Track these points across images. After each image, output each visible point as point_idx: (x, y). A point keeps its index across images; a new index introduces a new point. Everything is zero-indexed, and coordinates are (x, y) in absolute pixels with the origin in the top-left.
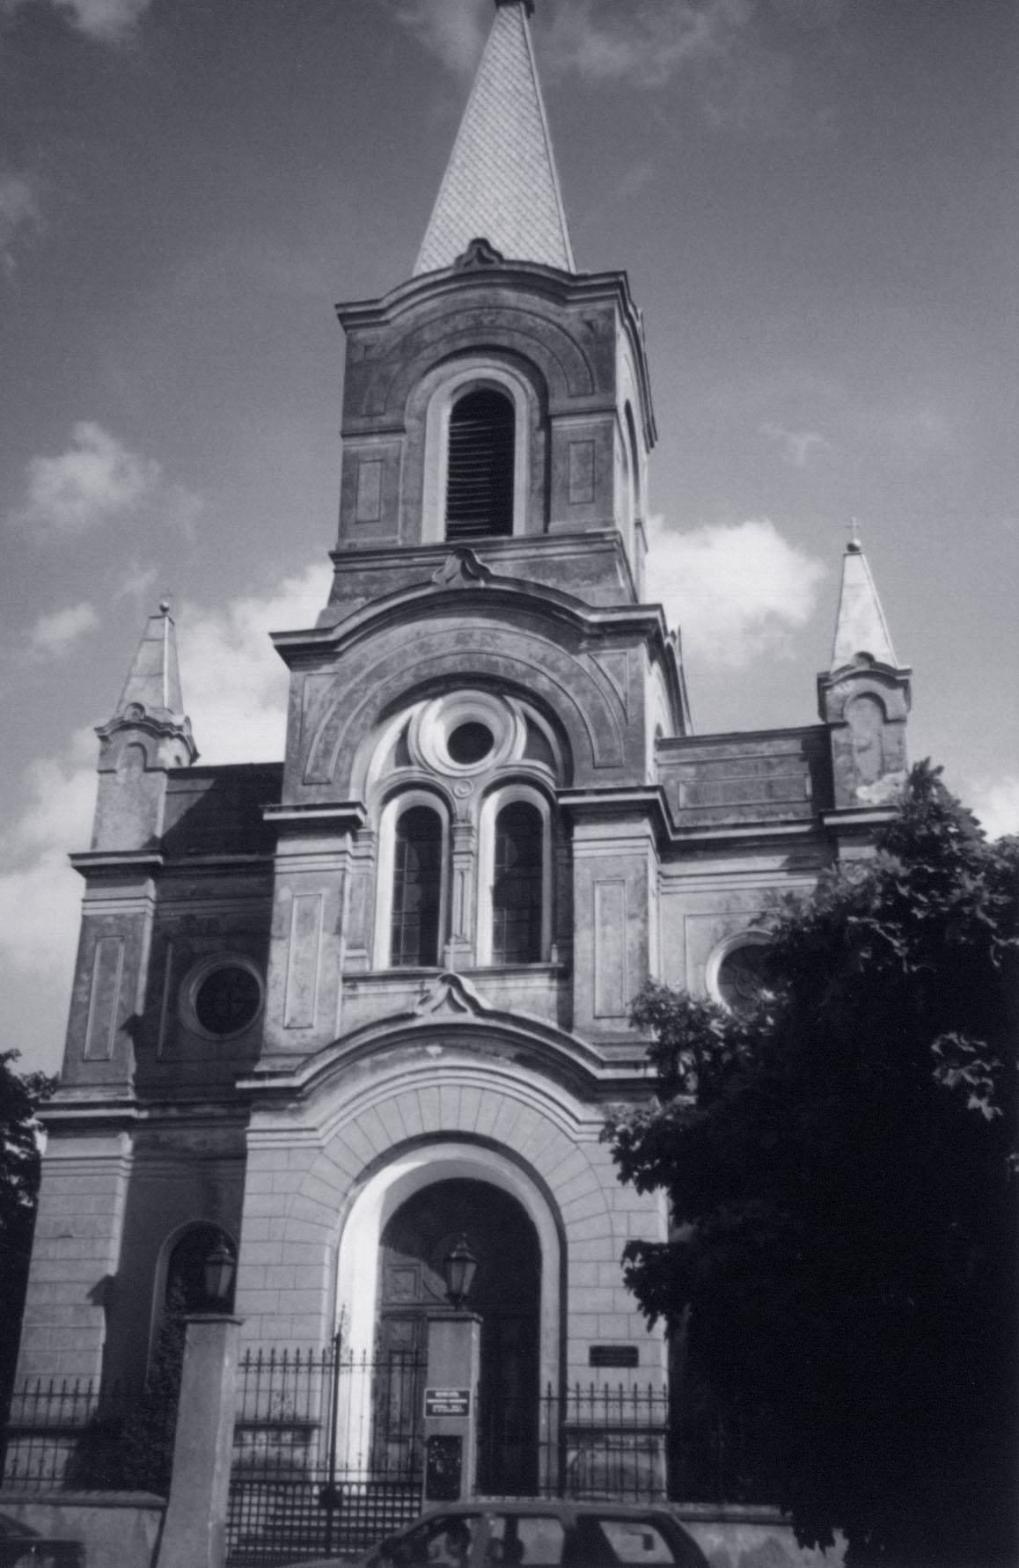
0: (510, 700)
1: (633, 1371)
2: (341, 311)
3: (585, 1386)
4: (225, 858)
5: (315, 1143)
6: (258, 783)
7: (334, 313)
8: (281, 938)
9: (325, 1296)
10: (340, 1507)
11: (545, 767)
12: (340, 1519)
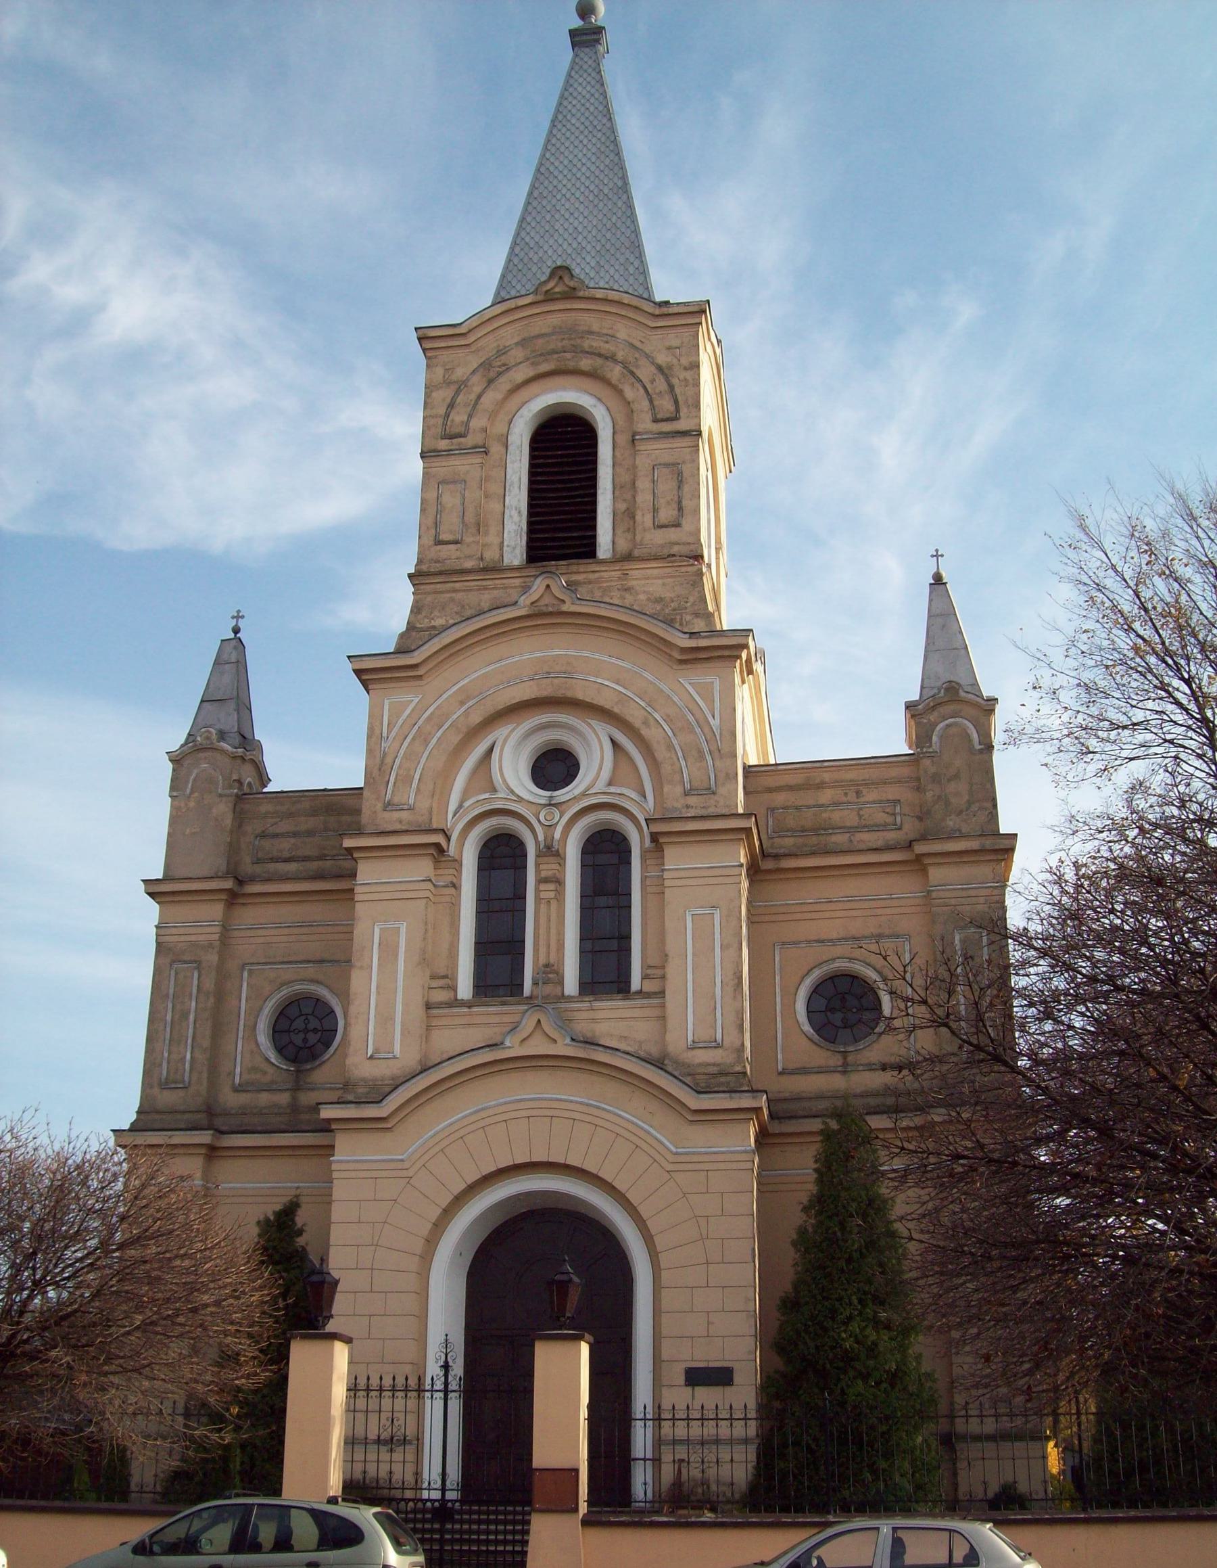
0: (593, 722)
1: (728, 1389)
2: (421, 332)
3: (681, 1406)
4: (747, 1025)
5: (405, 1173)
6: (334, 808)
7: (414, 336)
8: (361, 968)
9: (43, 1503)
10: (454, 1522)
11: (633, 795)
12: (453, 1531)
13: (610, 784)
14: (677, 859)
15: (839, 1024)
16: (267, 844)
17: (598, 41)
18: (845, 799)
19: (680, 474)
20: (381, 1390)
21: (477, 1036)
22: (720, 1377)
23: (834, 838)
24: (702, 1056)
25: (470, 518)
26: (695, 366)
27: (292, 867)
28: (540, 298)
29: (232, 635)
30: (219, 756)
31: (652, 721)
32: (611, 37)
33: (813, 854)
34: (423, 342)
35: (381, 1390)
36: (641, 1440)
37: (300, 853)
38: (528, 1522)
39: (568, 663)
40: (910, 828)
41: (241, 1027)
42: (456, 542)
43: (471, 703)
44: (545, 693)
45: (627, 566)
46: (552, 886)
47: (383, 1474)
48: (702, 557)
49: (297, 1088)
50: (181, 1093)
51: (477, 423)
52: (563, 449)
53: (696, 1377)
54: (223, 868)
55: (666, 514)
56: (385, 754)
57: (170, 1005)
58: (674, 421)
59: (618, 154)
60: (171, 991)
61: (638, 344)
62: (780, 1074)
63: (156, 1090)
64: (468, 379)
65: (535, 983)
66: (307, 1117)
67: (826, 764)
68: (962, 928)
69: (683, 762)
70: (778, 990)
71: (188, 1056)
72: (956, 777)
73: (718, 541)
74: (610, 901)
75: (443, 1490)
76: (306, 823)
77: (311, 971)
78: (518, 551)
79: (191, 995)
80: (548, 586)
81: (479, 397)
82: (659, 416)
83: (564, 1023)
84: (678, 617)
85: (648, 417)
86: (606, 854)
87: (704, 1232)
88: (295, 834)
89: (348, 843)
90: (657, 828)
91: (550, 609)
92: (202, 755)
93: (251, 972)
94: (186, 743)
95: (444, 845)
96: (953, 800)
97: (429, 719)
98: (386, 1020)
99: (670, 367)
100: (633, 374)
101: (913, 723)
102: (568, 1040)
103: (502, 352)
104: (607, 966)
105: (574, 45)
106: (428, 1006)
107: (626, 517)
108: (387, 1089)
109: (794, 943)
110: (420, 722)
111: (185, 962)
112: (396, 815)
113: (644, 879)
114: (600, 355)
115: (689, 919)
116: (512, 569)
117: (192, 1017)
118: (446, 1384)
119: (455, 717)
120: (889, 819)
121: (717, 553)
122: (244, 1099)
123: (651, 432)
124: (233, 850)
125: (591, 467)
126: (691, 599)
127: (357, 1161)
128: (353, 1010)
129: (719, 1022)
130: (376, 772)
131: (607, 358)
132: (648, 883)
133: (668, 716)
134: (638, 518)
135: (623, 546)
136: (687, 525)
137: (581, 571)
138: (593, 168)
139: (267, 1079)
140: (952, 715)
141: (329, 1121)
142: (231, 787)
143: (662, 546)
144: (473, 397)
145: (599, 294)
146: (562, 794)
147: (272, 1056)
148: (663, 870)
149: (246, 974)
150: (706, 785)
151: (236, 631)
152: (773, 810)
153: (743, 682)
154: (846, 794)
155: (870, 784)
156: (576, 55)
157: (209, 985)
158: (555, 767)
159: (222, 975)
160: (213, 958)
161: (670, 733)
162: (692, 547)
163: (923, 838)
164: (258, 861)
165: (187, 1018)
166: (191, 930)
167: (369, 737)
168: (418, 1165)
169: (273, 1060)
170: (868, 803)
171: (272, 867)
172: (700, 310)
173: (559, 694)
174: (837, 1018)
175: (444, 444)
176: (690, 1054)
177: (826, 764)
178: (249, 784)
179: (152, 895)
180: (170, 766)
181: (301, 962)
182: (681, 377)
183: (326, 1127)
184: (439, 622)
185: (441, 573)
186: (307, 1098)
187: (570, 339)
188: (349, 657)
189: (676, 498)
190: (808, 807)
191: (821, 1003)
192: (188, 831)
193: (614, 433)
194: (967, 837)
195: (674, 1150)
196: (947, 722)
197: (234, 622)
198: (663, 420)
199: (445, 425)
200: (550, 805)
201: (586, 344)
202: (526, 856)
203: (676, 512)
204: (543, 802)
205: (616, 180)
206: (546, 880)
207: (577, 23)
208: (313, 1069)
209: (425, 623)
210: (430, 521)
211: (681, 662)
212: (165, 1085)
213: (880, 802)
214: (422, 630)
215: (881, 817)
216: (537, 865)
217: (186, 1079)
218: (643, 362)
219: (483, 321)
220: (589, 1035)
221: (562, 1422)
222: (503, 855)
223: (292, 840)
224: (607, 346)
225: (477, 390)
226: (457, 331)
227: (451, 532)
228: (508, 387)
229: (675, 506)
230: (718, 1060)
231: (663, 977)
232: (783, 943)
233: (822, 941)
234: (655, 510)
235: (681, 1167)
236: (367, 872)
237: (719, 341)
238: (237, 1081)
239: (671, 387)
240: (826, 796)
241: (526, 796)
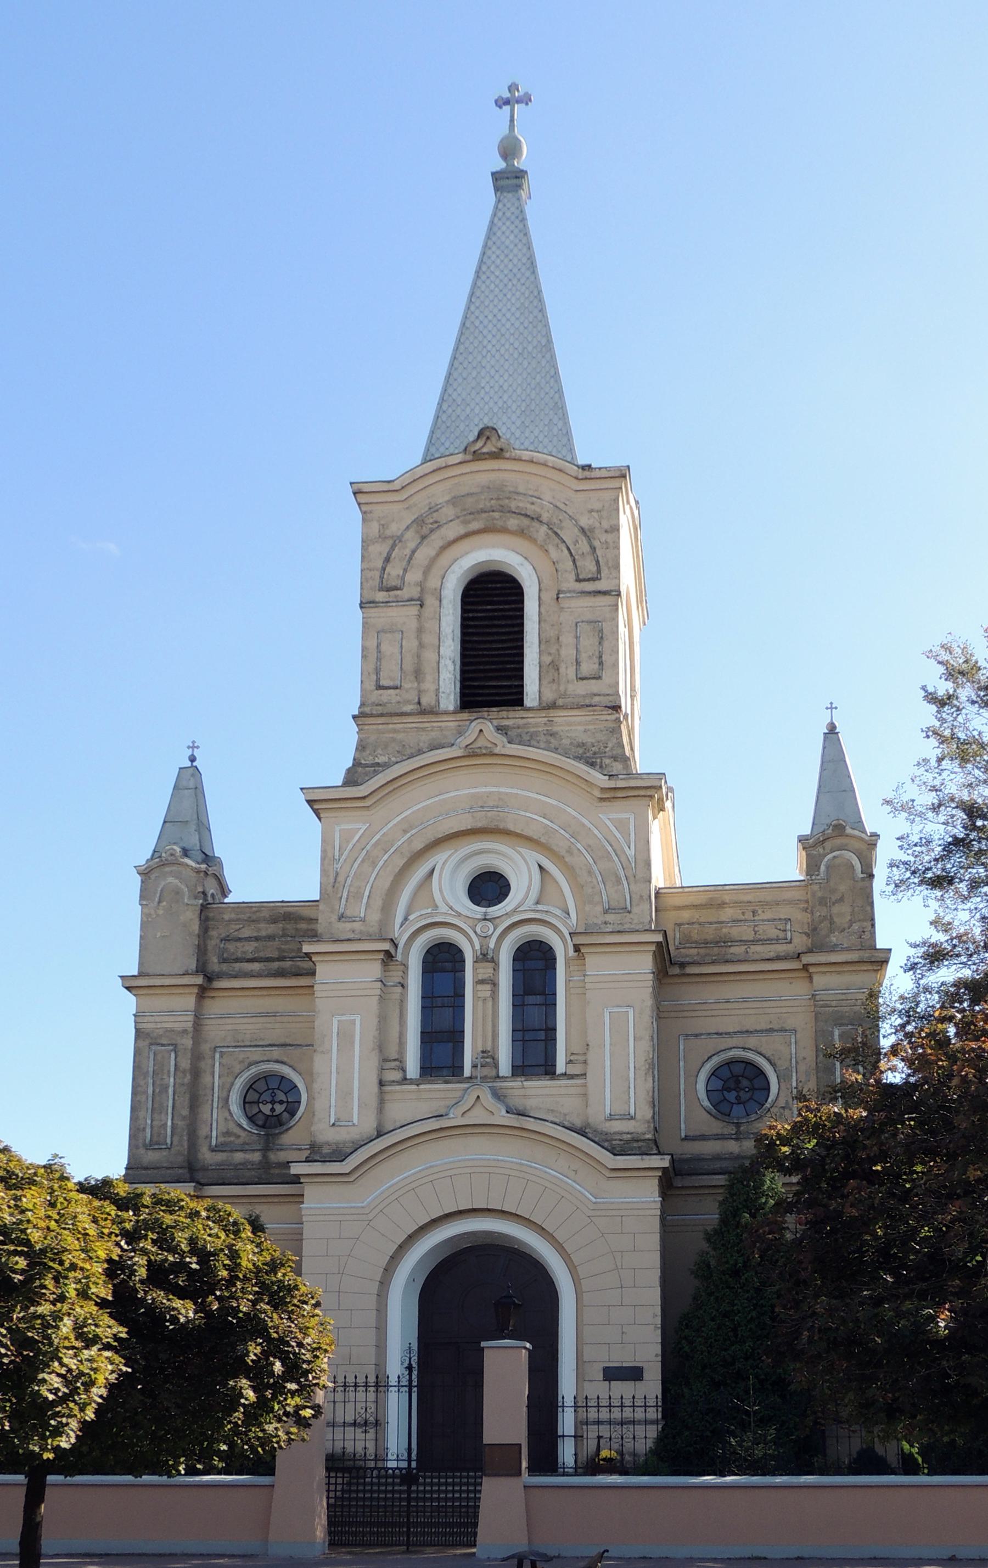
5: (364, 1217)
7: (350, 490)
8: (323, 1052)
10: (418, 1485)
11: (558, 912)
13: (537, 903)
14: (596, 964)
15: (733, 1100)
16: (231, 947)
17: (519, 186)
18: (743, 918)
19: (601, 631)
20: (356, 1386)
21: (424, 1109)
22: (635, 1374)
23: (732, 950)
24: (617, 1126)
25: (409, 665)
26: (615, 529)
27: (256, 966)
28: (469, 457)
29: (189, 764)
30: (183, 869)
31: (576, 851)
32: (533, 182)
33: (713, 962)
34: (358, 496)
35: (356, 1386)
36: (567, 1422)
37: (262, 954)
38: (481, 1484)
39: (500, 799)
40: (800, 942)
41: (216, 1099)
42: (396, 688)
43: (413, 832)
44: (479, 825)
45: (552, 713)
46: (488, 987)
47: (360, 1450)
48: (620, 707)
49: (266, 1149)
50: (165, 1153)
51: (414, 576)
52: (492, 607)
53: (612, 1374)
54: (194, 966)
55: (588, 667)
56: (337, 874)
57: (151, 1081)
58: (595, 578)
59: (542, 310)
60: (151, 1069)
61: (562, 506)
62: (682, 1140)
63: (142, 1151)
64: (402, 535)
65: (474, 1066)
66: (277, 1171)
67: (727, 888)
68: (841, 1025)
69: (602, 886)
70: (682, 1073)
71: (169, 1123)
72: (841, 900)
73: (633, 689)
74: (539, 999)
75: (409, 1460)
76: (266, 929)
77: (276, 1053)
78: (452, 697)
79: (169, 1071)
80: (481, 731)
81: (413, 552)
82: (581, 577)
83: (498, 1096)
84: (598, 760)
85: (572, 577)
86: (534, 963)
87: (619, 1264)
88: (257, 939)
89: (307, 948)
90: (579, 940)
91: (484, 751)
92: (167, 869)
93: (222, 1054)
94: (152, 858)
95: (393, 952)
96: (836, 920)
97: (375, 845)
98: (345, 1095)
99: (592, 530)
101: (804, 853)
102: (503, 1112)
103: (434, 509)
104: (535, 1049)
105: (497, 189)
106: (381, 1084)
107: (550, 669)
108: (349, 1151)
109: (696, 1035)
110: (368, 847)
111: (163, 1045)
112: (348, 926)
113: (567, 982)
114: (526, 516)
115: (607, 1016)
116: (446, 713)
117: (171, 1091)
118: (410, 1380)
119: (400, 843)
120: (781, 935)
121: (632, 700)
122: (220, 1157)
123: (574, 591)
124: (202, 951)
125: (518, 621)
126: (610, 745)
128: (316, 1086)
129: (632, 1101)
130: (330, 888)
131: (533, 519)
132: (571, 985)
133: (589, 846)
134: (562, 670)
135: (549, 696)
137: (511, 717)
138: (517, 324)
139: (240, 1141)
140: (837, 844)
141: (298, 1176)
142: (196, 898)
143: (584, 696)
144: (408, 552)
145: (526, 455)
146: (495, 911)
147: (244, 1123)
148: (584, 975)
149: (217, 1056)
150: (622, 905)
151: (193, 759)
152: (680, 925)
153: (655, 818)
156: (499, 201)
157: (185, 1064)
158: (488, 887)
159: (197, 1057)
160: (188, 1042)
161: (591, 861)
162: (611, 698)
163: (810, 951)
164: (225, 961)
165: (167, 1092)
166: (166, 1019)
167: (323, 859)
168: (377, 1211)
169: (245, 1126)
170: (763, 921)
171: (237, 966)
172: (622, 474)
173: (492, 825)
174: (732, 1096)
175: (381, 596)
176: (608, 1124)
177: (727, 888)
178: (213, 895)
179: (128, 988)
180: (139, 878)
181: (266, 1046)
182: (603, 540)
183: (296, 1180)
184: (382, 759)
185: (382, 715)
186: (273, 1157)
187: (498, 499)
188: (302, 789)
189: (597, 653)
190: (711, 923)
191: (718, 1084)
192: (159, 935)
193: (540, 590)
194: (848, 949)
195: (594, 1200)
196: (834, 854)
197: (189, 752)
198: (584, 580)
199: (382, 578)
200: (485, 919)
201: (513, 505)
202: (464, 961)
203: (597, 666)
204: (479, 917)
205: (539, 338)
206: (482, 982)
207: (500, 165)
208: (281, 1133)
209: (370, 760)
210: (371, 667)
212: (149, 1146)
214: (366, 766)
215: (773, 933)
216: (475, 969)
217: (169, 1141)
218: (567, 523)
219: (413, 480)
220: (521, 1108)
221: (504, 1415)
222: (443, 961)
223: (255, 944)
224: (533, 507)
225: (412, 545)
226: (391, 487)
227: (391, 679)
228: (440, 543)
229: (597, 661)
231: (585, 1062)
232: (687, 1035)
233: (721, 1034)
234: (578, 663)
235: (598, 1213)
236: (324, 971)
237: (637, 502)
238: (214, 1143)
239: (594, 549)
240: (728, 914)
241: (464, 912)
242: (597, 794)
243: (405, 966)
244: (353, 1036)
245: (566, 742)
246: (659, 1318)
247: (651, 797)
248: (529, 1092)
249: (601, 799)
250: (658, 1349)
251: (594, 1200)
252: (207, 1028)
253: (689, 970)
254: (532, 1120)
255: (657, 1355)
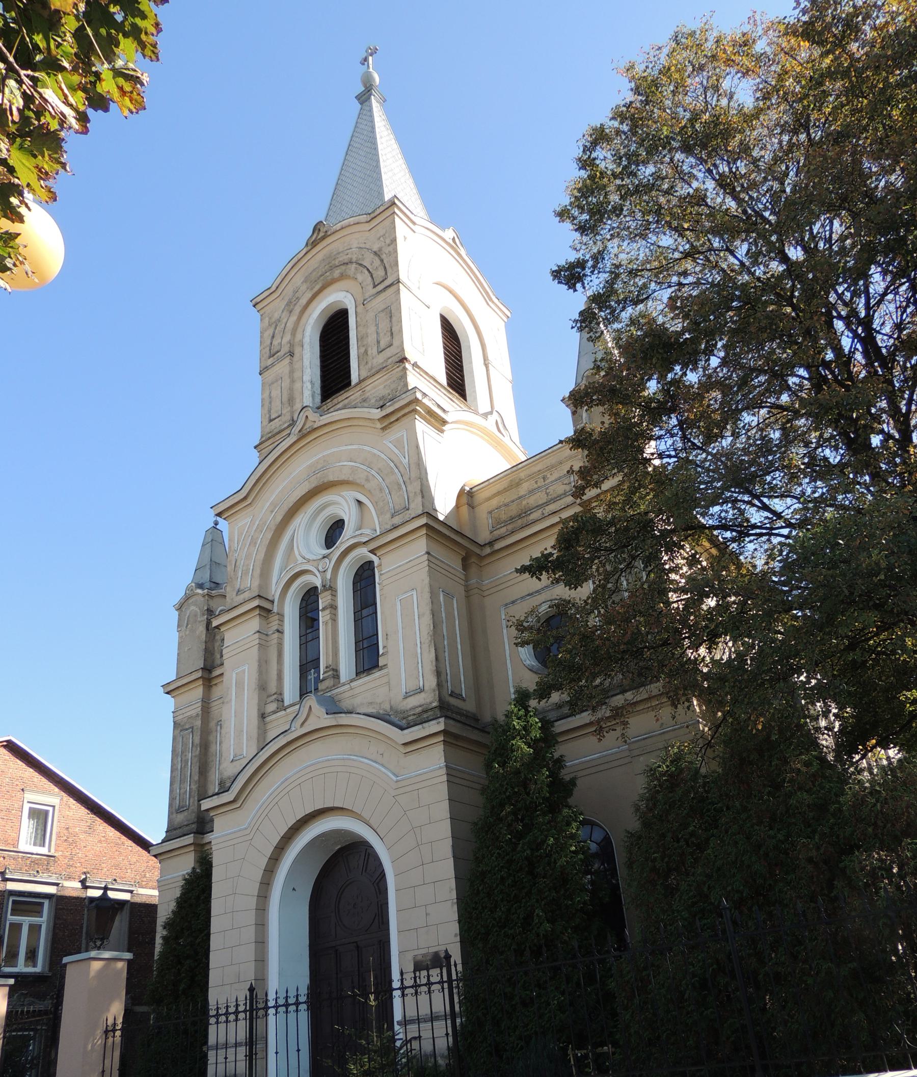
24: (413, 702)
28: (309, 248)
31: (371, 477)
50: (186, 813)
52: (335, 331)
63: (174, 815)
100: (361, 265)
107: (363, 357)
109: (513, 602)
115: (398, 604)
127: (223, 836)
128: (223, 731)
136: (396, 343)
145: (338, 226)
154: (536, 482)
155: (551, 468)
157: (197, 740)
160: (198, 723)
180: (177, 613)
201: (337, 263)
210: (266, 411)
211: (383, 429)
213: (560, 478)
225: (285, 320)
230: (422, 701)
233: (532, 594)
242: (379, 426)
243: (281, 615)
244: (244, 683)
245: (373, 401)
246: (455, 892)
247: (415, 411)
248: (356, 691)
249: (383, 429)
250: (455, 928)
251: (394, 778)
252: (213, 709)
253: (498, 546)
254: (343, 715)
255: (456, 935)
